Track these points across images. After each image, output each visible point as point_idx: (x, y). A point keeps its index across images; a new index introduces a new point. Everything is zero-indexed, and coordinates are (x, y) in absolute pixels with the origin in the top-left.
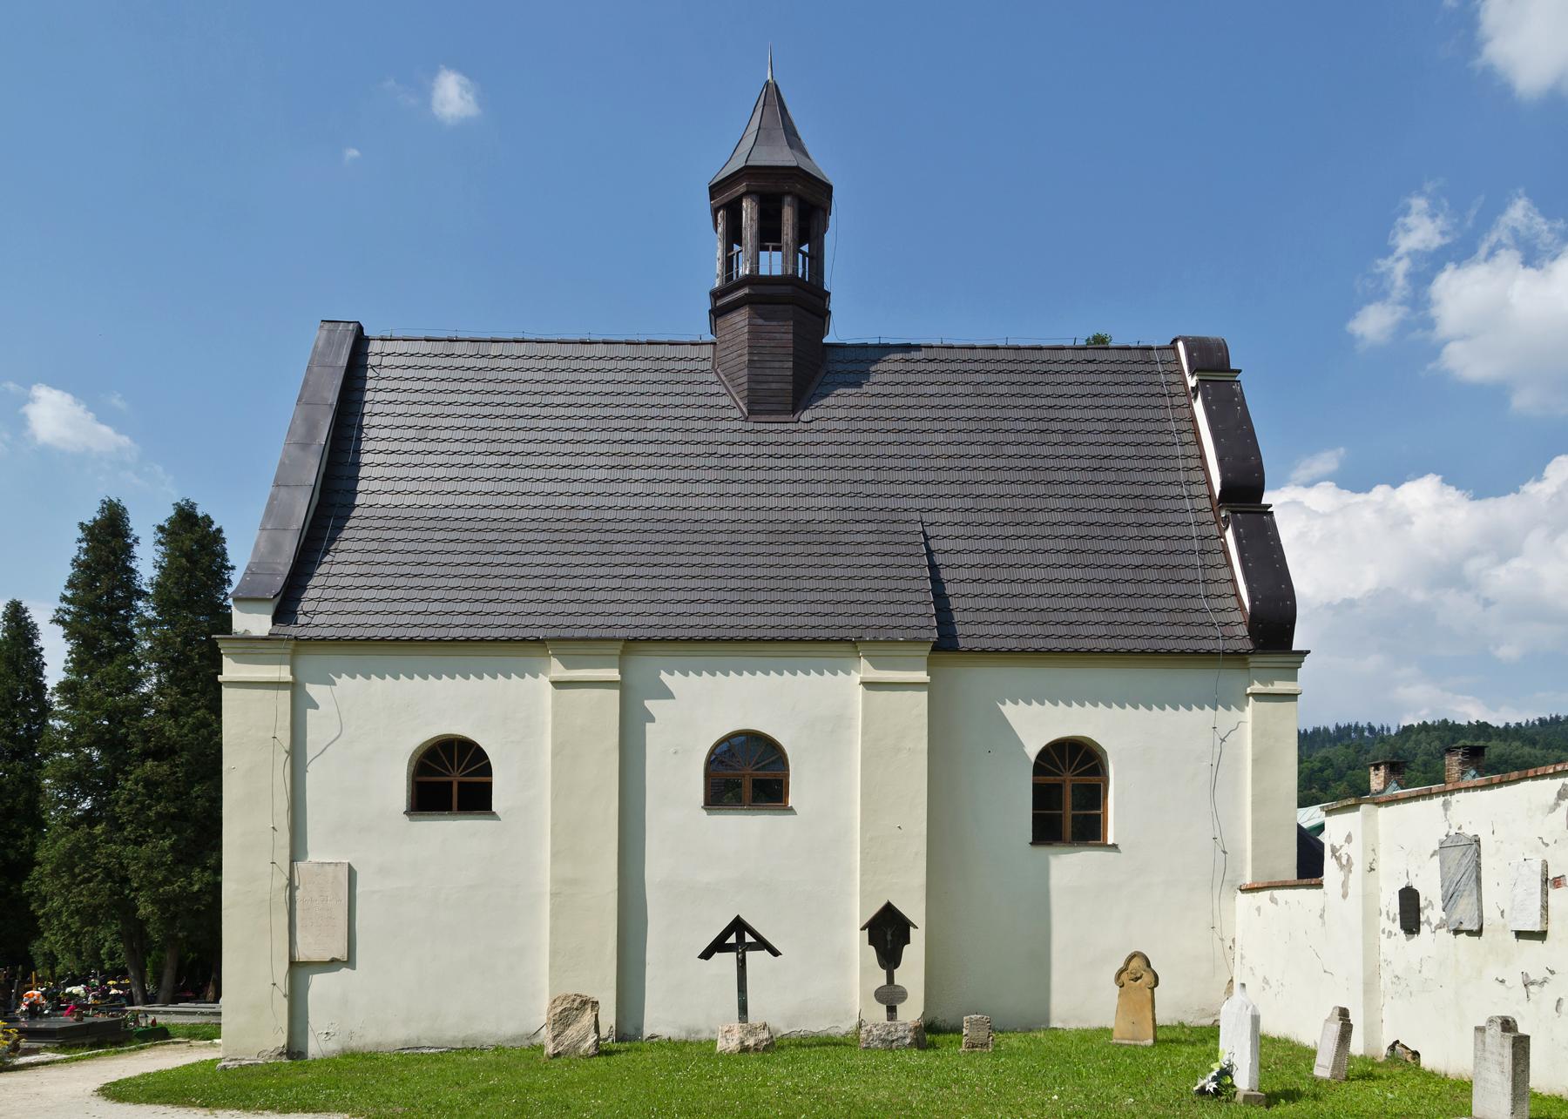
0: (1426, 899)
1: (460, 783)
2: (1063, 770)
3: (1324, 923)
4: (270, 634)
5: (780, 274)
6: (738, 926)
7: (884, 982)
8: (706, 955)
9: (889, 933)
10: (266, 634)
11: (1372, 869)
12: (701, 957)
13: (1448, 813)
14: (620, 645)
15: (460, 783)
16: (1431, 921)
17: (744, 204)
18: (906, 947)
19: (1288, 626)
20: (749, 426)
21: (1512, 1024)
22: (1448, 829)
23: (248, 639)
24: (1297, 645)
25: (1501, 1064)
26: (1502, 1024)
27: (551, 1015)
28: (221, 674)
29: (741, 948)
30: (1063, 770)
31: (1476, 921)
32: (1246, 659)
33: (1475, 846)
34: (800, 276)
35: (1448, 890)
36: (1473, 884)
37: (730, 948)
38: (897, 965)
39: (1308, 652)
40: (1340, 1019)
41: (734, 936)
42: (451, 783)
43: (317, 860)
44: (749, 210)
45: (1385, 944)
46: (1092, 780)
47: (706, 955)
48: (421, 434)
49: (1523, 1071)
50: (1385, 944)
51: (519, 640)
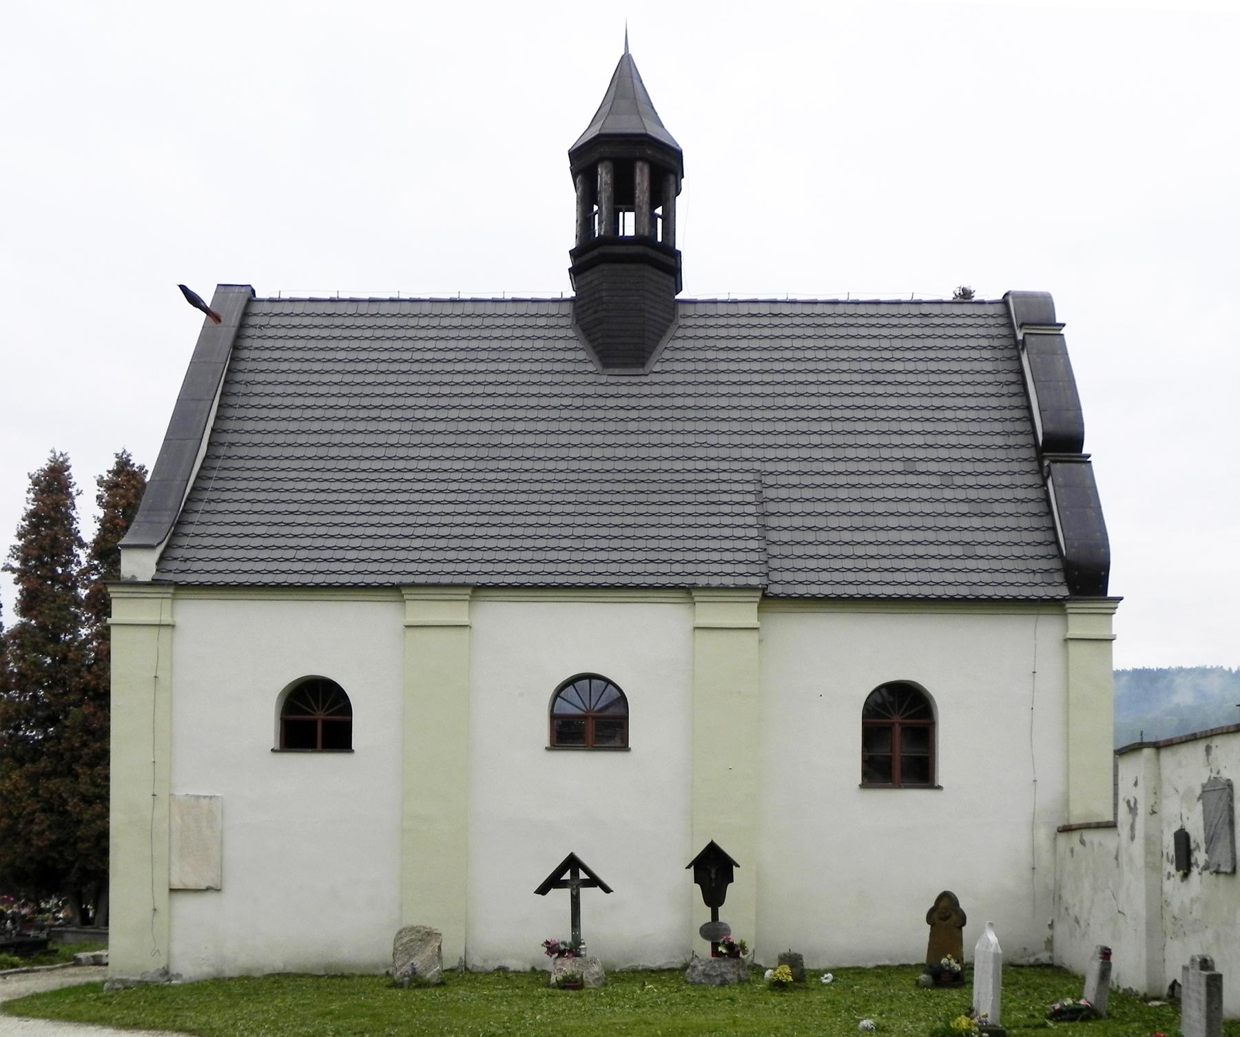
0: (1195, 842)
1: (325, 723)
2: (901, 712)
3: (1118, 864)
4: (153, 580)
5: (633, 234)
6: (572, 863)
7: (709, 919)
8: (543, 890)
9: (713, 871)
10: (148, 579)
11: (1154, 812)
12: (538, 892)
13: (1210, 757)
14: (469, 591)
15: (325, 723)
16: (1199, 863)
17: (599, 169)
18: (730, 886)
19: (1103, 573)
20: (603, 379)
21: (1210, 963)
22: (1209, 772)
23: (133, 583)
24: (1111, 593)
25: (1199, 1001)
26: (1201, 962)
27: (398, 944)
28: (110, 617)
29: (576, 887)
30: (901, 712)
31: (1229, 864)
32: (1064, 605)
33: (1228, 790)
34: (660, 239)
35: (1209, 833)
36: (1227, 828)
37: (564, 884)
38: (721, 903)
39: (1121, 599)
40: (1101, 958)
41: (586, 877)
42: (314, 723)
43: (195, 794)
44: (604, 176)
45: (1168, 885)
46: (922, 721)
47: (543, 890)
48: (947, 481)
49: (1216, 1008)
50: (1168, 885)
51: (362, 586)
